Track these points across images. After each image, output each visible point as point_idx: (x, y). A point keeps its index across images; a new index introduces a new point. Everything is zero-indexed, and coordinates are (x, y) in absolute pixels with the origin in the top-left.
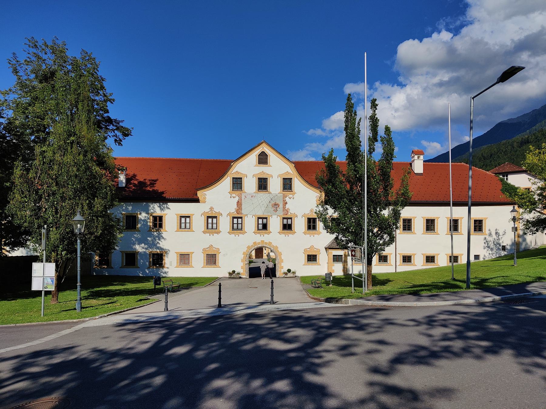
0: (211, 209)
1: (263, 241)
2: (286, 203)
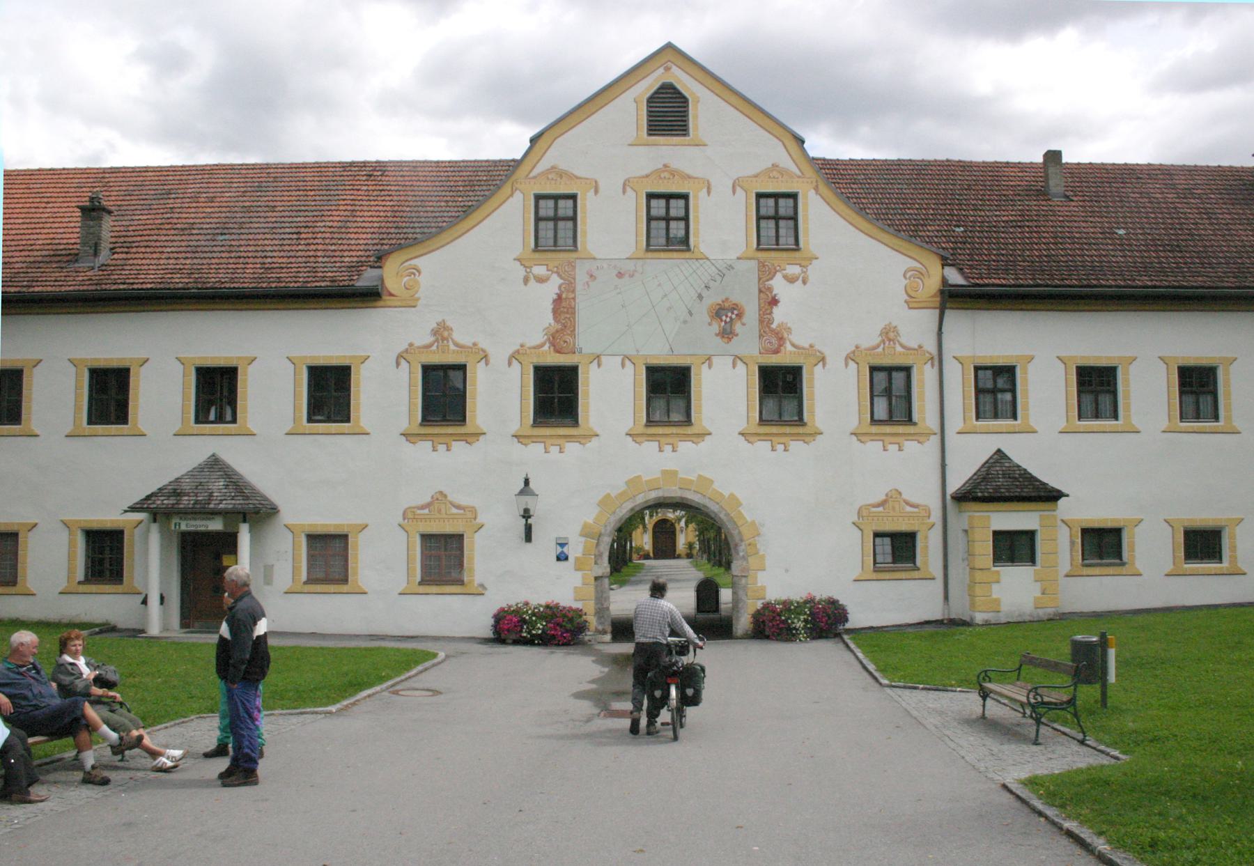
0: (441, 333)
1: (670, 475)
2: (774, 302)
